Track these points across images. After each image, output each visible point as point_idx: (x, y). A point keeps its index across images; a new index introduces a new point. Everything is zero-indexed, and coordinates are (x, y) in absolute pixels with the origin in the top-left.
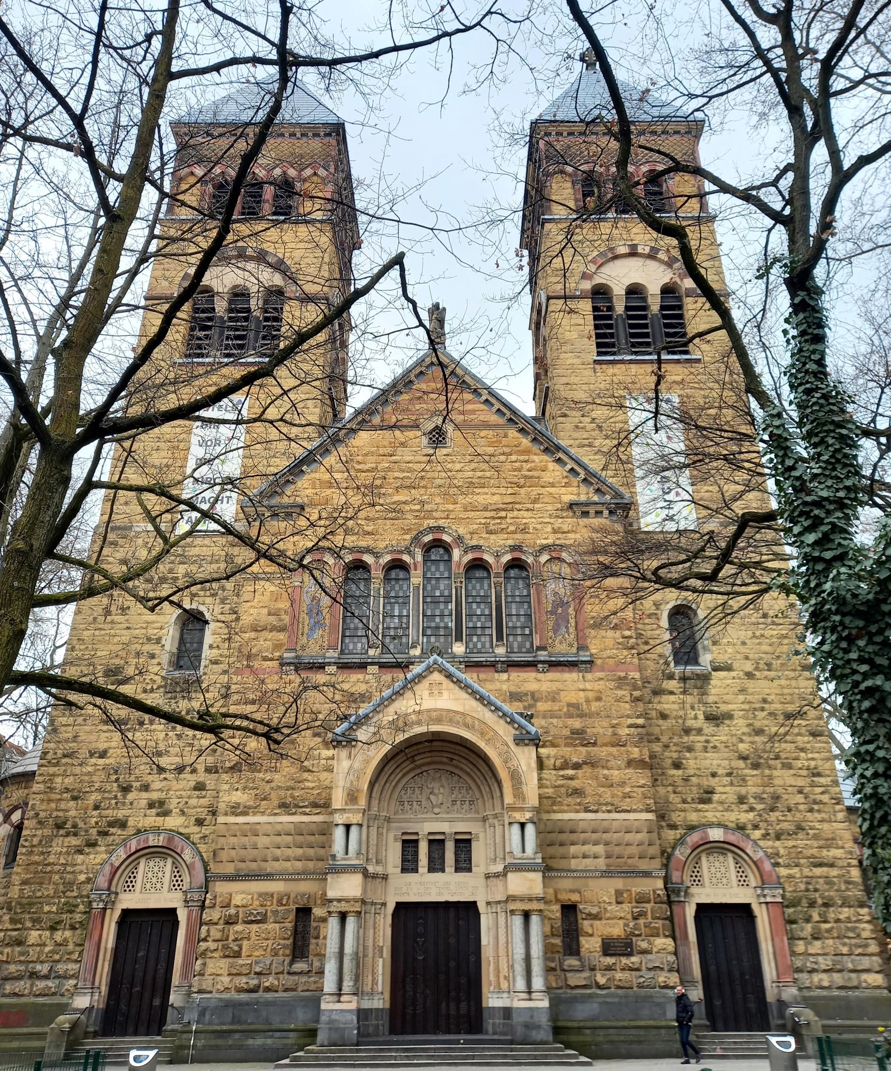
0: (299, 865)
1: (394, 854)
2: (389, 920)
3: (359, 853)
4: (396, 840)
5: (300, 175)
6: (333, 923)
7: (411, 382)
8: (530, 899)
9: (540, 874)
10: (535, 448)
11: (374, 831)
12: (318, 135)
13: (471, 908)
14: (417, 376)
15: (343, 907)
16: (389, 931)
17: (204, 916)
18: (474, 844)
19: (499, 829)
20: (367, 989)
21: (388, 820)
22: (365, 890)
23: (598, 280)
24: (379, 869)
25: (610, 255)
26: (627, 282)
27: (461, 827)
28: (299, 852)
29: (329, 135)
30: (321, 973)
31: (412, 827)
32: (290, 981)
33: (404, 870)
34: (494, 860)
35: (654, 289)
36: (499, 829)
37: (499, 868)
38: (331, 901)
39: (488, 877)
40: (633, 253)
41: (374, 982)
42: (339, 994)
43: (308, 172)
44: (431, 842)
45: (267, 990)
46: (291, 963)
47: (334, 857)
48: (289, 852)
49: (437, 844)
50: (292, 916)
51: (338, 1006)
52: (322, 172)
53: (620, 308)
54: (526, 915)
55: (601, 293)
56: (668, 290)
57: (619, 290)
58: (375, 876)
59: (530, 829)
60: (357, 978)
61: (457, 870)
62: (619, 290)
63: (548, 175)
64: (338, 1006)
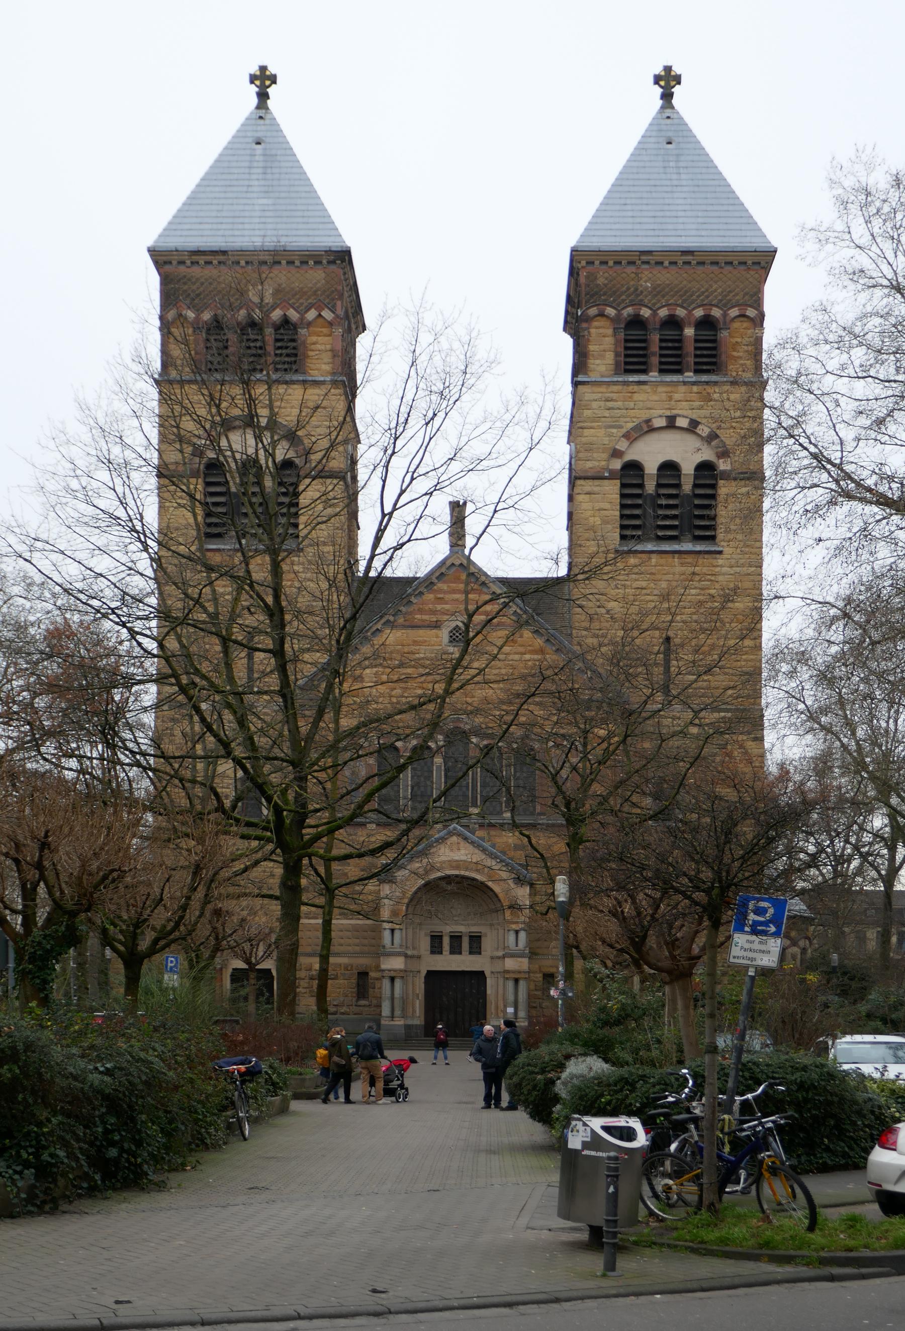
0: (357, 948)
1: (425, 944)
2: (423, 980)
3: (401, 946)
4: (426, 935)
6: (386, 983)
8: (520, 972)
11: (410, 931)
15: (393, 974)
16: (423, 986)
17: (262, 655)
21: (420, 924)
22: (406, 964)
24: (415, 953)
25: (646, 429)
27: (474, 929)
30: (379, 1006)
31: (438, 928)
32: (357, 1009)
33: (432, 952)
34: (497, 949)
35: (688, 468)
37: (500, 953)
39: (492, 958)
40: (671, 424)
41: (414, 1011)
42: (392, 1017)
43: (311, 315)
44: (451, 937)
45: (343, 1014)
47: (384, 947)
50: (356, 976)
52: (327, 314)
53: (650, 487)
55: (634, 468)
57: (651, 468)
58: (412, 957)
59: (522, 935)
60: (403, 1010)
61: (471, 953)
62: (651, 468)
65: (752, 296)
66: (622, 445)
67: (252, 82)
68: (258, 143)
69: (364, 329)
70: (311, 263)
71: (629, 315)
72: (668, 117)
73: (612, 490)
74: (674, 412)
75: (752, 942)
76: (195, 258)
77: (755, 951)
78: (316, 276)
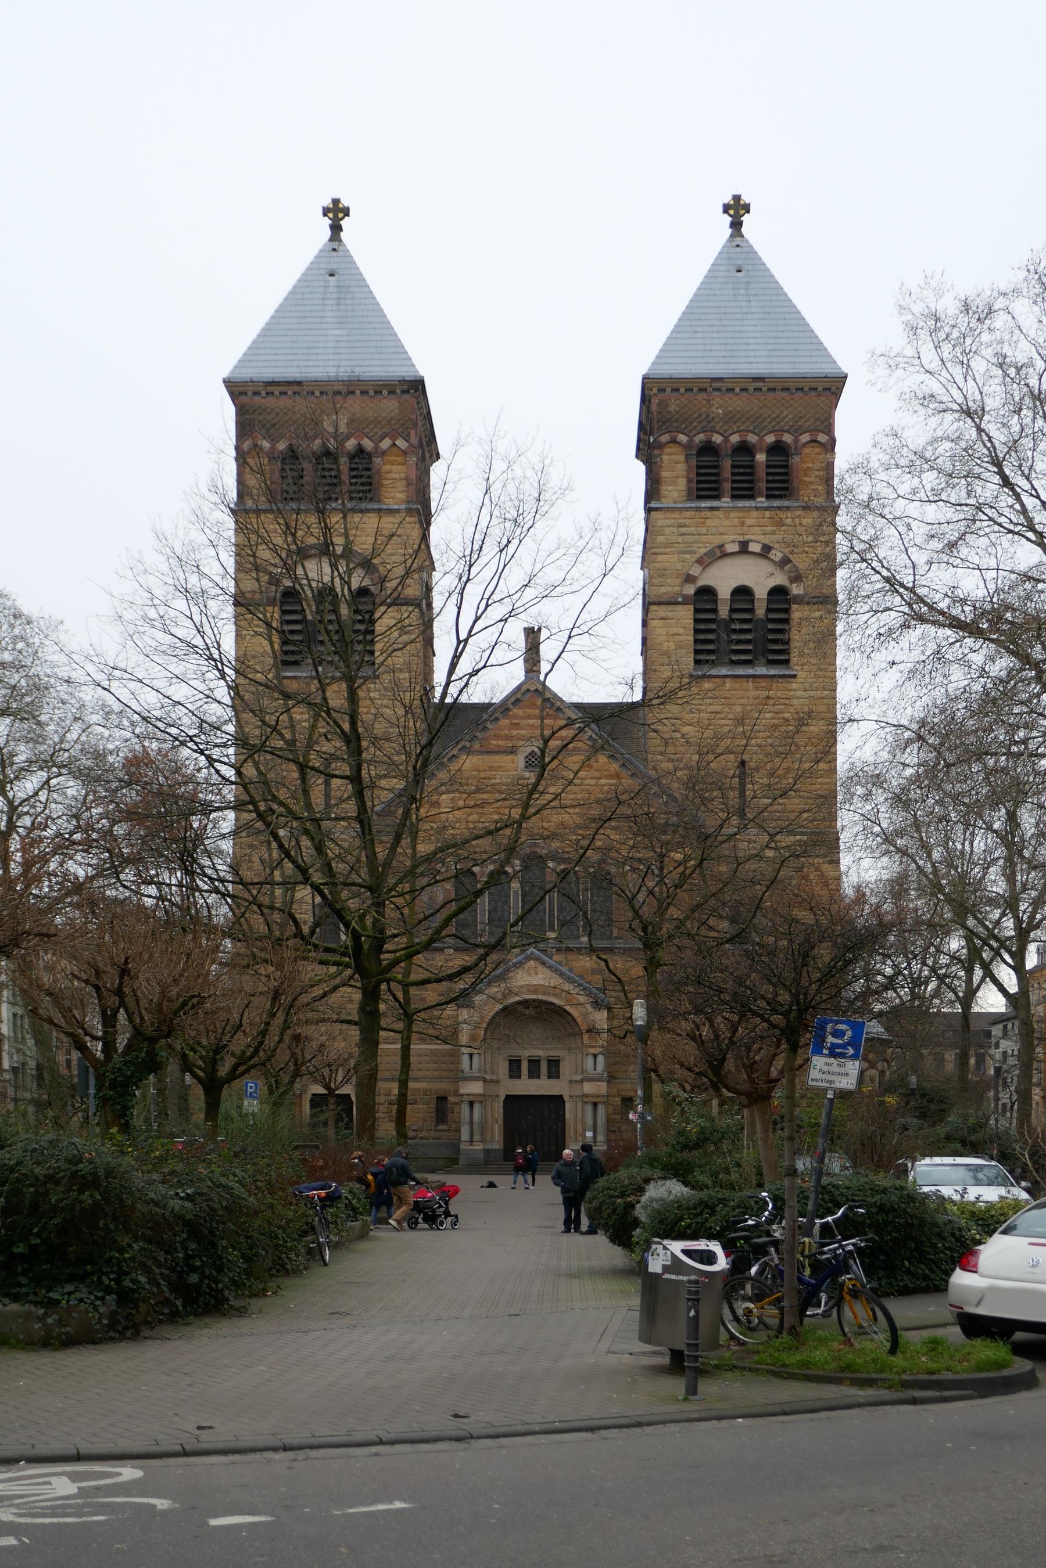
1: (503, 1068)
3: (479, 1070)
5: (377, 447)
6: (465, 1109)
7: (507, 709)
8: (598, 1096)
9: (605, 1084)
10: (625, 773)
11: (488, 1056)
12: (394, 392)
13: (559, 1100)
14: (513, 704)
18: (561, 1063)
19: (579, 1056)
20: (489, 1138)
21: (499, 1049)
22: (484, 1089)
23: (701, 583)
24: (494, 1077)
26: (734, 584)
27: (552, 1053)
28: (436, 1066)
29: (407, 392)
30: (458, 1131)
32: (436, 1135)
33: (511, 1077)
35: (761, 593)
36: (579, 1056)
37: (579, 1077)
38: (462, 1095)
39: (571, 1082)
40: (744, 549)
41: (493, 1136)
42: (472, 1141)
43: (386, 444)
44: (530, 1061)
45: (422, 1138)
46: (437, 1125)
47: (462, 1071)
48: (428, 1066)
49: (534, 1063)
51: (471, 1147)
52: (401, 443)
54: (595, 1105)
55: (707, 593)
56: (778, 593)
57: (724, 593)
58: (491, 1081)
59: (601, 1059)
62: (724, 593)
63: (661, 446)
64: (471, 1147)
65: (823, 422)
66: (695, 571)
67: (325, 215)
68: (332, 275)
69: (438, 457)
70: (385, 392)
71: (701, 442)
72: (738, 246)
73: (686, 615)
74: (747, 537)
75: (830, 1065)
76: (270, 389)
77: (833, 1074)
78: (390, 406)
